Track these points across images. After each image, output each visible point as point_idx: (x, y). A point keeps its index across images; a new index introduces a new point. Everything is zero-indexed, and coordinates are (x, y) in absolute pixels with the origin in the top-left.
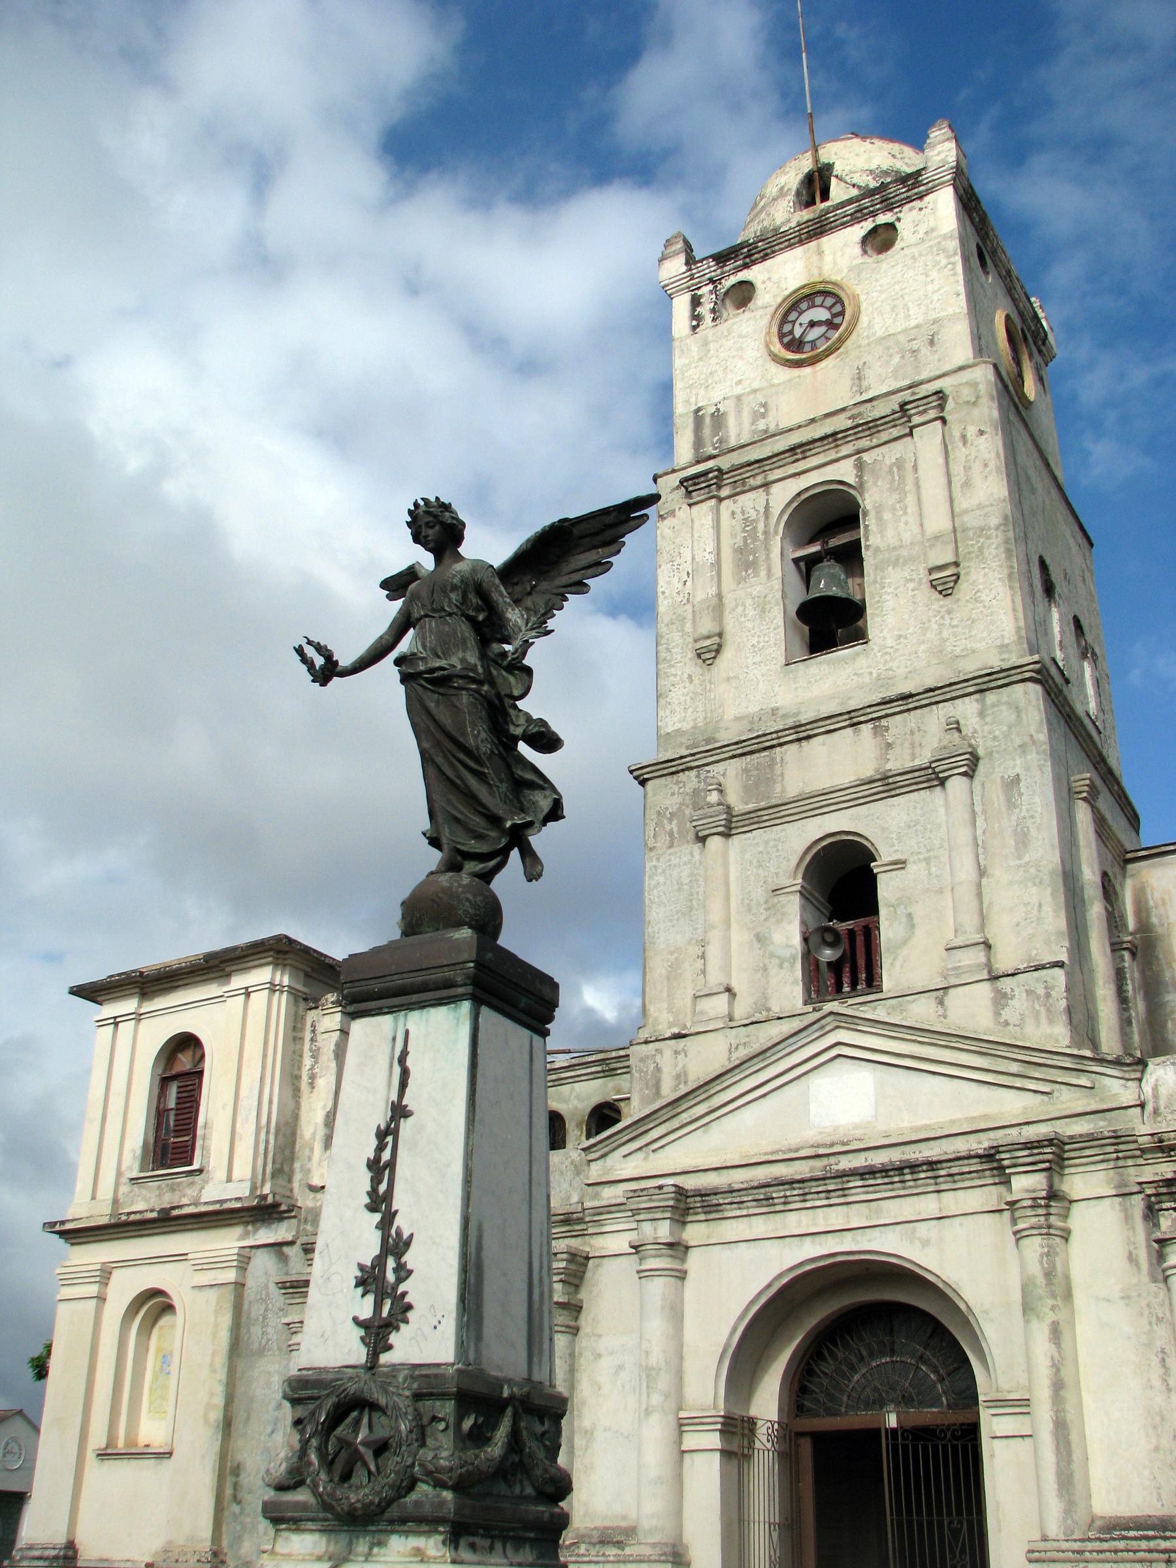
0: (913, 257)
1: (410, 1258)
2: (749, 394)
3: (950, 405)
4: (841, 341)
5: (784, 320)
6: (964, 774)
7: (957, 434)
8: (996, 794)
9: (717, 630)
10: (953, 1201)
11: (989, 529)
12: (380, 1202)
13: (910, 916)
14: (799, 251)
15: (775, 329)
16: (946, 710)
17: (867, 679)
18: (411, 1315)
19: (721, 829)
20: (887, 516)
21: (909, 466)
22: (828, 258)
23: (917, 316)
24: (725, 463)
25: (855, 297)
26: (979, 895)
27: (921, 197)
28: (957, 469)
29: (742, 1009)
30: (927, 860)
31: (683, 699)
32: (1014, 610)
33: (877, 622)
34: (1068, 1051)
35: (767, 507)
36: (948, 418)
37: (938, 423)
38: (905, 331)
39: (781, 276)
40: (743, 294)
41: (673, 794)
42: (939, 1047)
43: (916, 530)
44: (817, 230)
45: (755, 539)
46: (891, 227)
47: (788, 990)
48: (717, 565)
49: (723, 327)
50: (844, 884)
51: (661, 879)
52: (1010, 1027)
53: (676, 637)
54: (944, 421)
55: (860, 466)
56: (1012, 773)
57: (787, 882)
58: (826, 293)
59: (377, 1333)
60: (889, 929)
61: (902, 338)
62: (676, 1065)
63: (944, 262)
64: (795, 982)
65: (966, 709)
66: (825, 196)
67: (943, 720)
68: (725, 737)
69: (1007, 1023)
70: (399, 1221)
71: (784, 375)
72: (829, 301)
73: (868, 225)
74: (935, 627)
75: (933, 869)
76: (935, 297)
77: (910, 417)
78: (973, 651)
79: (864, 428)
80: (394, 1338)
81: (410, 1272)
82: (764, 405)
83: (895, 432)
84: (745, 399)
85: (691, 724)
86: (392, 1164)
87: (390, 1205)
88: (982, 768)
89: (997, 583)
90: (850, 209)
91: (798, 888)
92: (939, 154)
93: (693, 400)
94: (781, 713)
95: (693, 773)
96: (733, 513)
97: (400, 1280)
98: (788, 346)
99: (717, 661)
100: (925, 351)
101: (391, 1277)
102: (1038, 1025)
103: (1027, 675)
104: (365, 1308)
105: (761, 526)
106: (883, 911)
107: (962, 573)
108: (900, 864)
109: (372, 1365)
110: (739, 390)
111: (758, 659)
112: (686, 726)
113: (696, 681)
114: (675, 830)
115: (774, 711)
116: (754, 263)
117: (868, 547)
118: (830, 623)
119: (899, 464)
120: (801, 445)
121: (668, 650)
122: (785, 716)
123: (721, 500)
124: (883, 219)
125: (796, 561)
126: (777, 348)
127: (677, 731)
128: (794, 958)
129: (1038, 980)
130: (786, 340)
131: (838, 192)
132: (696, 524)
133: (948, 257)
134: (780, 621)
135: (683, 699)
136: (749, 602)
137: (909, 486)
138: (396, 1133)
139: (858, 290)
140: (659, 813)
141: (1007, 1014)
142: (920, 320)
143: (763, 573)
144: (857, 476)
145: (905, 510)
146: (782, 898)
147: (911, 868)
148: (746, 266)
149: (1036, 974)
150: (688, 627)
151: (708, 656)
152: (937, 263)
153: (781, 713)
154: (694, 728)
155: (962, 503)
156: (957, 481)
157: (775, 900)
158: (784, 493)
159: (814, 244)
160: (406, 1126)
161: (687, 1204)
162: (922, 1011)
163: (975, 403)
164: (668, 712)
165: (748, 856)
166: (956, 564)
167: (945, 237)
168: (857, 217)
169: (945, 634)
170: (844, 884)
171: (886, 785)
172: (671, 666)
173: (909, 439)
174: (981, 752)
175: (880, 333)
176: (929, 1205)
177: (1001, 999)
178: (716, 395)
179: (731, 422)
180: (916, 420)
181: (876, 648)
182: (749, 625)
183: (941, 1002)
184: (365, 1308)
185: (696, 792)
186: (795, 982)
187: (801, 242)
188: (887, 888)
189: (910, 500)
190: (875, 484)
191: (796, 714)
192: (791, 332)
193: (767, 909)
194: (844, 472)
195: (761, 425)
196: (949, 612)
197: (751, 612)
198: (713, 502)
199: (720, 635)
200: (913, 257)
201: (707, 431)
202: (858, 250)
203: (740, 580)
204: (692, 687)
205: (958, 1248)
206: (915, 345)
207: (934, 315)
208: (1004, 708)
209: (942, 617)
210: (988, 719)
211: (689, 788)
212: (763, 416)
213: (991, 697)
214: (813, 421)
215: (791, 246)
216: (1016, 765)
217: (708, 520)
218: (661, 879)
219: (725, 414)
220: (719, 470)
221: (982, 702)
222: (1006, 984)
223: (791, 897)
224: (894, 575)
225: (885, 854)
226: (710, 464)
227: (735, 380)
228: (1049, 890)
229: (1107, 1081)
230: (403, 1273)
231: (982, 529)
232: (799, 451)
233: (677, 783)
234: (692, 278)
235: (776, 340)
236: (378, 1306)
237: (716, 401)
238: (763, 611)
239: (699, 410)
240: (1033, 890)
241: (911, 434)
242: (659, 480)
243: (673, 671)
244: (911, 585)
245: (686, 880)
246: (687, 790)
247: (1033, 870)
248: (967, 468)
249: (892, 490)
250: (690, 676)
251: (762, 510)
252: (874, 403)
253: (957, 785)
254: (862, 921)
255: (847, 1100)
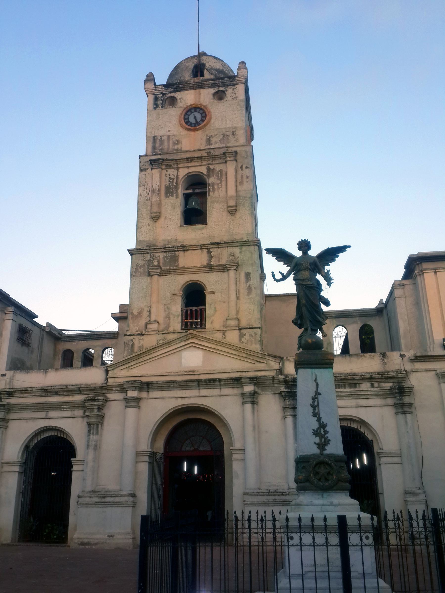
0: (230, 104)
1: (327, 429)
2: (173, 136)
3: (238, 157)
4: (205, 126)
5: (186, 114)
6: (235, 269)
7: (240, 166)
8: (243, 276)
9: (159, 211)
10: (225, 391)
11: (247, 198)
12: (316, 414)
13: (215, 308)
14: (192, 92)
15: (183, 116)
16: (229, 250)
17: (206, 236)
18: (330, 442)
19: (158, 274)
20: (216, 187)
21: (224, 173)
22: (202, 97)
23: (229, 125)
24: (165, 157)
25: (210, 112)
26: (237, 305)
27: (234, 85)
28: (239, 177)
29: (162, 327)
30: (221, 292)
31: (146, 231)
32: (252, 223)
33: (210, 219)
34: (260, 352)
35: (177, 175)
36: (238, 160)
37: (235, 162)
38: (225, 128)
39: (188, 98)
40: (173, 101)
41: (142, 260)
42: (220, 346)
43: (225, 193)
44: (200, 86)
45: (173, 185)
46: (224, 92)
47: (176, 324)
48: (159, 191)
49: (165, 111)
50: (194, 297)
51: (137, 286)
52: (244, 344)
53: (145, 210)
54: (236, 161)
55: (209, 169)
56: (249, 271)
57: (178, 293)
58: (200, 109)
59: (322, 446)
60: (209, 311)
61: (224, 130)
62: (140, 343)
63: (239, 109)
64: (178, 322)
65: (236, 250)
66: (202, 75)
67: (229, 252)
68: (160, 244)
69: (243, 343)
70: (323, 420)
71: (184, 132)
72: (201, 112)
73: (216, 90)
74: (228, 224)
75: (223, 295)
76: (236, 120)
77: (226, 157)
78: (239, 233)
79: (211, 156)
80: (326, 447)
81: (328, 432)
82: (178, 141)
83: (220, 161)
84: (171, 138)
85: (148, 239)
86: (318, 405)
87: (319, 416)
88: (239, 269)
89: (248, 215)
90: (211, 82)
91: (181, 295)
92: (242, 72)
93: (153, 133)
94: (178, 241)
95: (149, 255)
96: (166, 175)
97: (325, 434)
98: (187, 123)
99: (158, 221)
100: (231, 136)
101: (323, 433)
102: (252, 344)
103: (255, 244)
104: (317, 440)
105: (175, 181)
106: (207, 305)
107: (238, 209)
108: (213, 292)
109: (322, 454)
110: (169, 133)
111: (171, 223)
112: (147, 239)
113: (151, 226)
114: (142, 271)
115: (176, 240)
116: (177, 91)
117: (209, 195)
118: (194, 215)
119: (221, 171)
120: (190, 158)
121: (142, 214)
122: (179, 242)
123: (162, 169)
124: (221, 89)
125: (184, 194)
126: (183, 123)
127: (144, 240)
128: (178, 316)
129: (253, 331)
130: (186, 121)
131: (207, 75)
132: (154, 176)
133: (241, 107)
134: (180, 213)
135: (146, 231)
136: (169, 204)
137: (224, 179)
138: (317, 398)
139: (212, 110)
140: (136, 265)
141: (244, 340)
142: (230, 126)
143: (175, 196)
144: (207, 172)
145: (221, 186)
146: (176, 297)
147: (216, 294)
148: (175, 92)
149: (252, 330)
150: (149, 208)
151: (155, 219)
152: (238, 108)
153: (178, 241)
154: (149, 240)
155: (240, 188)
156: (239, 180)
157: (174, 297)
158: (183, 172)
159: (198, 90)
160: (320, 397)
161: (147, 386)
162: (218, 336)
163: (246, 158)
164: (141, 234)
165: (165, 283)
166: (236, 206)
167: (241, 101)
168: (213, 86)
169: (231, 227)
170: (194, 297)
171: (210, 268)
172: (142, 219)
173: (224, 164)
174: (239, 263)
175: (217, 127)
176: (216, 392)
177: (241, 336)
178: (161, 133)
179: (166, 144)
180: (228, 159)
181: (209, 227)
182: (169, 211)
183: (224, 334)
184: (317, 440)
185: (149, 261)
186: (178, 322)
187: (193, 89)
188: (209, 298)
189: (224, 183)
190: (213, 176)
191: (183, 242)
192: (188, 118)
193: (171, 300)
194: (203, 170)
195: (176, 147)
196: (233, 220)
197: (170, 208)
198: (160, 170)
199: (160, 213)
200: (230, 104)
201: (157, 145)
202: (212, 97)
203: (167, 197)
204: (149, 227)
205: (226, 406)
206: (228, 134)
207: (235, 126)
208: (247, 252)
209: (230, 222)
210: (242, 254)
211: (147, 259)
212: (177, 144)
213: (244, 248)
214: (194, 151)
215: (190, 89)
216: (249, 269)
217: (158, 175)
218: (137, 286)
219: (164, 140)
220: (163, 160)
221: (241, 249)
222: (244, 331)
223: (179, 297)
224: (216, 205)
225: (209, 288)
226: (159, 157)
227: (168, 130)
228: (257, 306)
229: (270, 362)
230: (326, 432)
231: (245, 197)
232: (190, 160)
233: (144, 257)
234: (156, 90)
235: (183, 120)
236: (321, 440)
237: (161, 135)
238: (174, 208)
239: (154, 137)
240: (252, 305)
241: (226, 162)
242: (141, 158)
243: (143, 221)
244: (221, 210)
245: (145, 287)
246: (147, 259)
247: (252, 300)
248: (242, 177)
249: (218, 179)
250: (149, 224)
251: (176, 176)
252: (215, 150)
253: (232, 273)
254: (198, 308)
255: (192, 359)
